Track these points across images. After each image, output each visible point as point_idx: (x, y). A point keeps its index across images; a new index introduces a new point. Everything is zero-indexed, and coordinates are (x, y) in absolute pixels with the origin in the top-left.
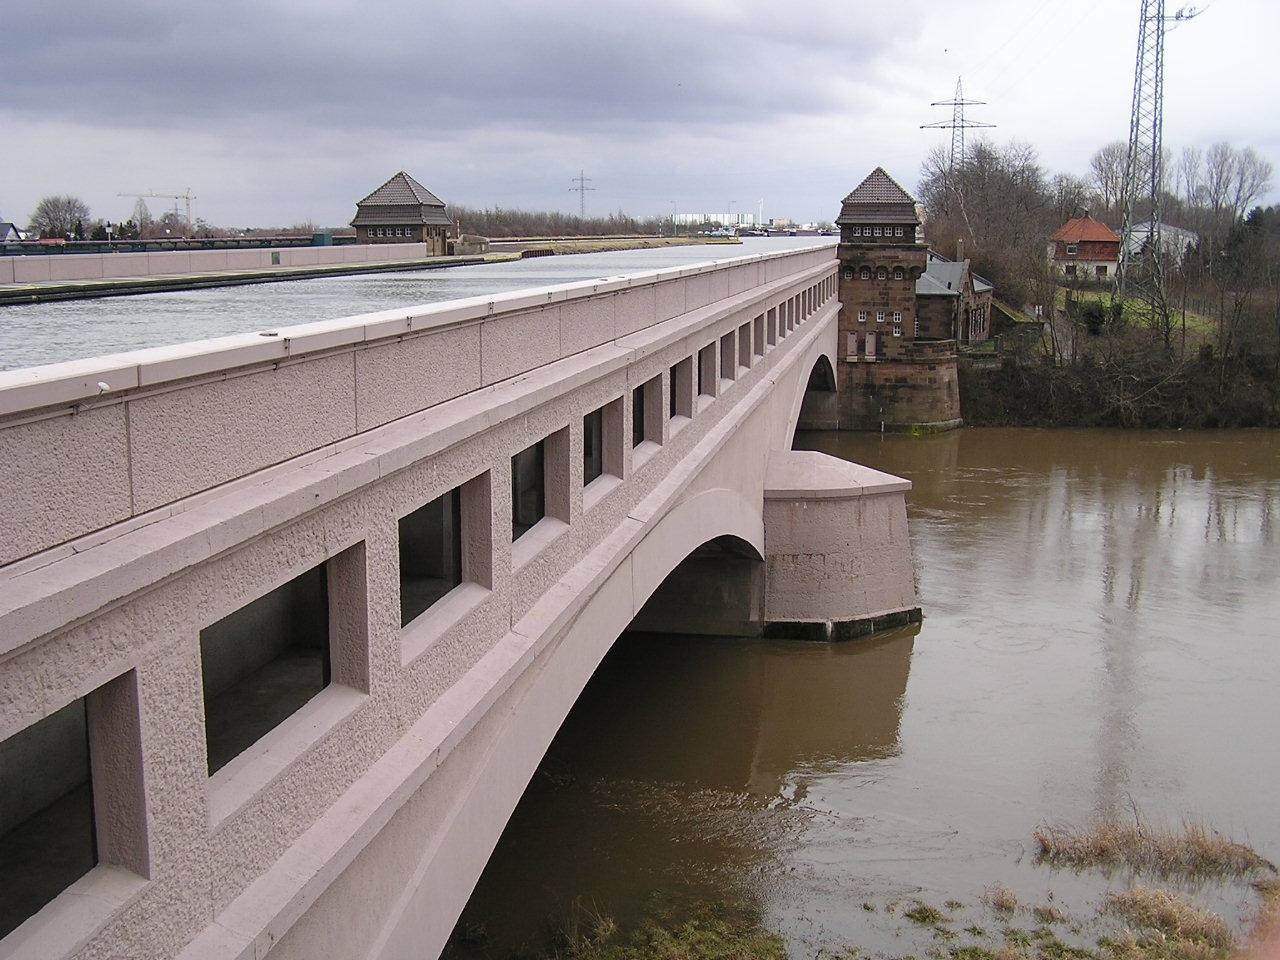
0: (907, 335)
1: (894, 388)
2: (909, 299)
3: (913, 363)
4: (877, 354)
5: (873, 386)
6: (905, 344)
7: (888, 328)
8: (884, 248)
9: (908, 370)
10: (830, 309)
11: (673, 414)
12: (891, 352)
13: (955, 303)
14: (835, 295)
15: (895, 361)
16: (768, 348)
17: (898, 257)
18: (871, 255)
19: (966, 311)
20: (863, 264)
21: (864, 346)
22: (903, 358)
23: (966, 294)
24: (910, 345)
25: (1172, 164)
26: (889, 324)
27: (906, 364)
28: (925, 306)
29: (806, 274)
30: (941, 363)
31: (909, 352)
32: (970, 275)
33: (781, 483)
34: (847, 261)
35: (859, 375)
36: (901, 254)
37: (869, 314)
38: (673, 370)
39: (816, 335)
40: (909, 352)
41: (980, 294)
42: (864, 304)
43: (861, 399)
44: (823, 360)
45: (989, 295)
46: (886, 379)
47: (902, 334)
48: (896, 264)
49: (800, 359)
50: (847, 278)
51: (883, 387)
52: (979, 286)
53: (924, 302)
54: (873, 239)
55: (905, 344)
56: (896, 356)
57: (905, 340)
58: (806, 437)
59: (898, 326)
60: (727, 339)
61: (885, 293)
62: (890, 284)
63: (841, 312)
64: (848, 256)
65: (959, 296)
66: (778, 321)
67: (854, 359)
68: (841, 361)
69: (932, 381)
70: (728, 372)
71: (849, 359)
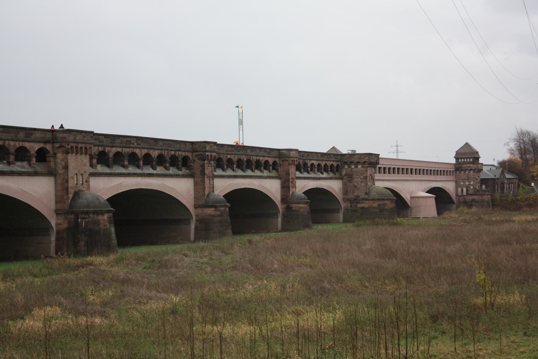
1: (471, 202)
8: (467, 164)
9: (475, 197)
15: (471, 195)
18: (464, 166)
35: (462, 199)
59: (472, 185)
61: (468, 176)
64: (457, 166)
68: (457, 195)
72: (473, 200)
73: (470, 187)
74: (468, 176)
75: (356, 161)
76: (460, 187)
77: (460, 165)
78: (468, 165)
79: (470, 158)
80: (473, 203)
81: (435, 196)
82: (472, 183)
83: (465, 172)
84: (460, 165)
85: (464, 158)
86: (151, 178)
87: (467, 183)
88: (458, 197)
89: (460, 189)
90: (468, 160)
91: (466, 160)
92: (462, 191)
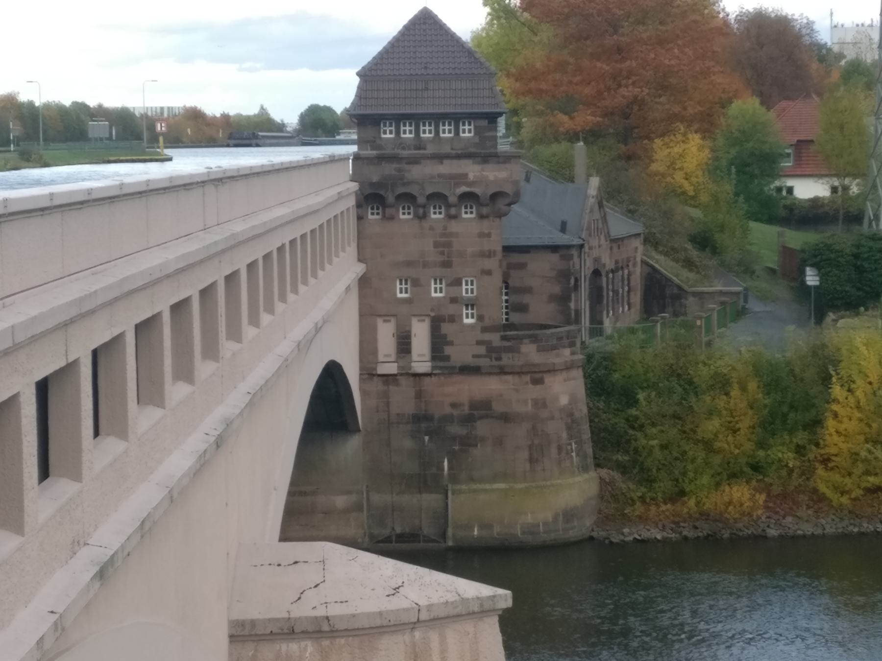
0: (487, 322)
1: (468, 420)
2: (490, 254)
3: (502, 371)
4: (434, 358)
5: (428, 418)
6: (487, 337)
7: (451, 309)
8: (440, 158)
10: (344, 270)
11: (97, 433)
12: (461, 353)
13: (576, 259)
14: (352, 250)
15: (468, 370)
16: (227, 347)
17: (466, 175)
18: (416, 172)
19: (596, 273)
20: (401, 190)
21: (409, 344)
22: (484, 362)
23: (594, 242)
24: (495, 338)
25: (653, 531)
26: (454, 300)
27: (490, 374)
28: (522, 266)
29: (109, 280)
30: (552, 370)
31: (492, 351)
32: (601, 206)
33: (269, 603)
34: (372, 185)
35: (403, 401)
36: (472, 170)
37: (416, 283)
38: (95, 353)
39: (320, 322)
40: (492, 351)
41: (617, 242)
42: (409, 264)
43: (408, 444)
44: (332, 373)
45: (637, 243)
46: (453, 405)
47: (480, 318)
48: (464, 189)
49: (286, 367)
50: (372, 217)
51: (447, 419)
52: (620, 225)
53: (516, 258)
54: (419, 144)
55: (487, 337)
56: (469, 360)
57: (485, 330)
58: (301, 519)
59: (470, 304)
60: (146, 328)
61: (444, 245)
62: (454, 226)
63: (363, 282)
64: (375, 175)
65: (582, 246)
66: (333, 249)
67: (391, 368)
68: (368, 373)
69: (540, 404)
70: (151, 392)
71: (383, 369)
72: (482, 409)
73: (453, 319)
74: (444, 245)
75: (430, 190)
76: (386, 317)
77: (389, 169)
78: (448, 168)
79: (456, 119)
80: (483, 428)
81: (503, 597)
82: (466, 290)
83: (422, 217)
84: (389, 169)
85: (416, 119)
86: (245, 168)
87: (436, 292)
88: (377, 386)
89: (386, 343)
90: (408, 134)
91: (408, 134)
92: (404, 345)
